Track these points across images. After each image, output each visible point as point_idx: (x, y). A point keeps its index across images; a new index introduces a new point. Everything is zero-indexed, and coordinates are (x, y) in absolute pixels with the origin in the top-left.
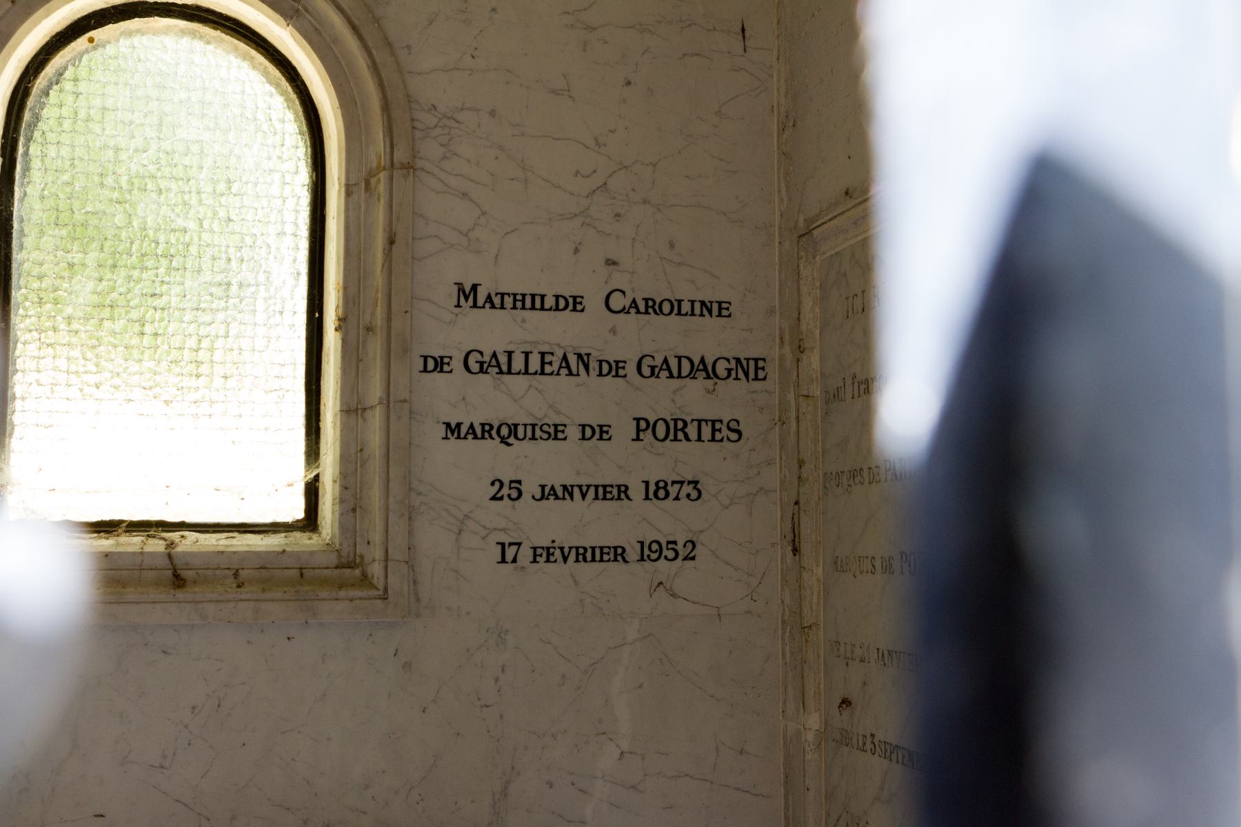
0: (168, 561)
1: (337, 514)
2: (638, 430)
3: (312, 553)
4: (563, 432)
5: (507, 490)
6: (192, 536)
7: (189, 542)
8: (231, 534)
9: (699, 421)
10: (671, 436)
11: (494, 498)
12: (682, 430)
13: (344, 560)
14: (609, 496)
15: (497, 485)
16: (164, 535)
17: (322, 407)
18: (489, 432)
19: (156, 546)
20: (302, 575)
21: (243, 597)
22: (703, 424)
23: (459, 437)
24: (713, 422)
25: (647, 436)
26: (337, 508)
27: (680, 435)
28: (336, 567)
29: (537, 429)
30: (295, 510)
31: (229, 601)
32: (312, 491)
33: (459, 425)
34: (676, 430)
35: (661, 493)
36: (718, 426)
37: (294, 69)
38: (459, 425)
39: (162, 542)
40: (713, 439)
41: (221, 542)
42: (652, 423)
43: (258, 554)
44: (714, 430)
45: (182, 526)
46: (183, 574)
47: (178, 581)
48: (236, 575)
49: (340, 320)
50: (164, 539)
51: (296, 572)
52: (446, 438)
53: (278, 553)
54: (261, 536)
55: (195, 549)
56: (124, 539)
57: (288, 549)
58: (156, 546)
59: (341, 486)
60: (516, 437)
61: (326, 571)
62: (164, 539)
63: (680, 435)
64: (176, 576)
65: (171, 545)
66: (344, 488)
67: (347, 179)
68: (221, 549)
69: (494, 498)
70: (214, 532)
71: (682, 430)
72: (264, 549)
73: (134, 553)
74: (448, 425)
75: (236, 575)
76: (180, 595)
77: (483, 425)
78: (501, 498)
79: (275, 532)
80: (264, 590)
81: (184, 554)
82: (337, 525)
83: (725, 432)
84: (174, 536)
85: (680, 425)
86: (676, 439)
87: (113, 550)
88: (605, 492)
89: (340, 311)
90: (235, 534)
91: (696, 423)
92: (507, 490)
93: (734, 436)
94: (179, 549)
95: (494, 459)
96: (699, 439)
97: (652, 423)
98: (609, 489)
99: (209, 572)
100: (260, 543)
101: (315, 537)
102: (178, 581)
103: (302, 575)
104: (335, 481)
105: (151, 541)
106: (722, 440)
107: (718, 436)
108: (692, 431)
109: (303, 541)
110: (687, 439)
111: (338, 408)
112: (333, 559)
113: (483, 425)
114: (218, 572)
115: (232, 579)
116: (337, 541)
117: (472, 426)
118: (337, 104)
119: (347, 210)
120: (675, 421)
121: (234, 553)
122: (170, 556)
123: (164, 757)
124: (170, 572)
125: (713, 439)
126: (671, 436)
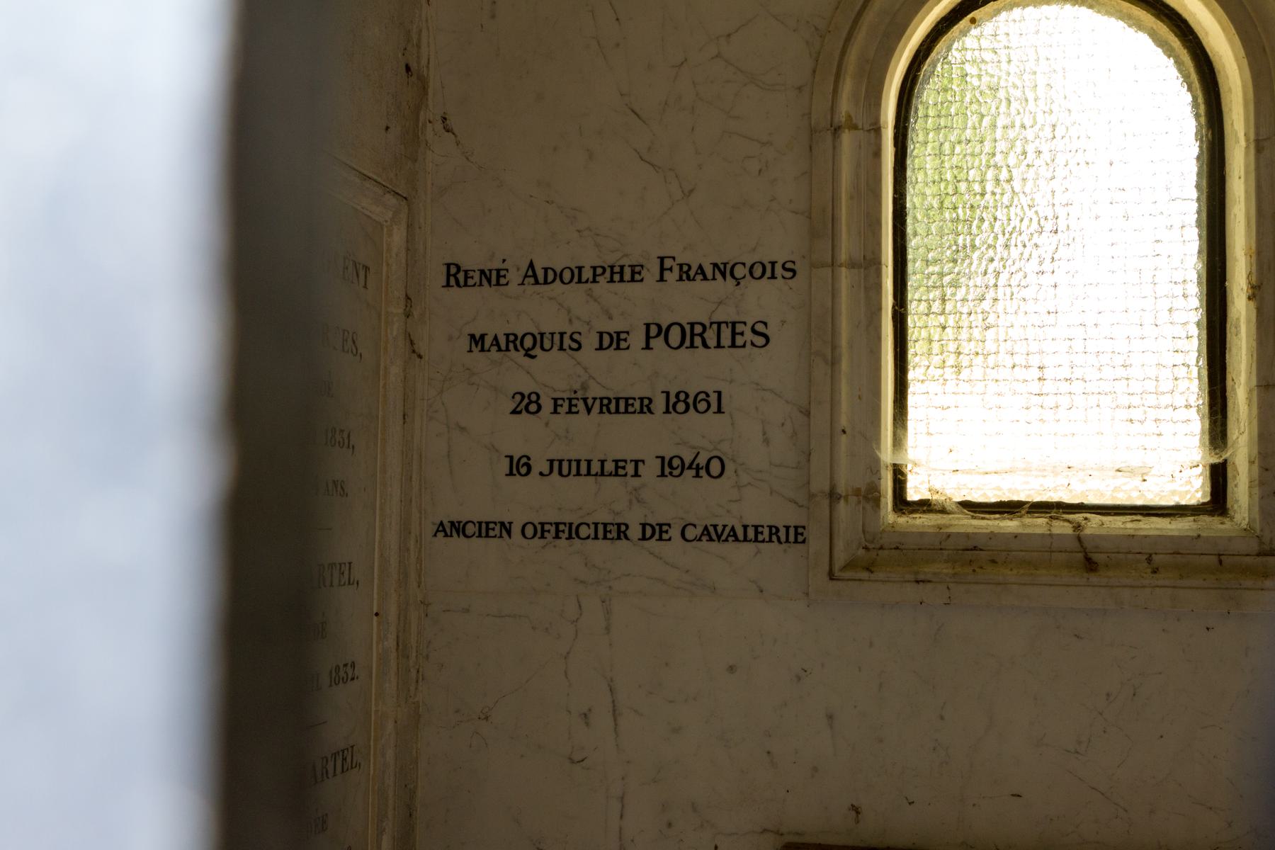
0: (1077, 544)
1: (1256, 498)
2: (648, 338)
3: (1230, 539)
4: (625, 340)
5: (527, 404)
6: (1095, 519)
7: (1095, 523)
8: (1135, 517)
9: (719, 324)
10: (687, 343)
11: (514, 412)
12: (701, 335)
13: (1267, 547)
14: (631, 409)
15: (518, 397)
16: (1071, 517)
17: (1229, 383)
18: (514, 342)
19: (1062, 528)
20: (1221, 562)
21: (1160, 583)
22: (723, 326)
23: (482, 350)
24: (734, 324)
25: (658, 343)
26: (1256, 490)
27: (698, 341)
28: (1258, 555)
29: (566, 338)
30: (1194, 490)
31: (1144, 587)
32: (1219, 476)
33: (482, 336)
34: (693, 335)
35: (681, 407)
36: (739, 328)
37: (1185, 22)
38: (482, 336)
39: (1066, 524)
40: (733, 345)
41: (1129, 525)
42: (664, 328)
43: (1171, 538)
44: (734, 334)
45: (1081, 508)
46: (1095, 557)
47: (1090, 565)
48: (1149, 560)
49: (1253, 287)
50: (1068, 521)
51: (1214, 559)
52: (470, 351)
53: (1192, 538)
54: (1168, 520)
55: (1103, 532)
56: (1028, 520)
57: (1203, 534)
58: (1062, 528)
59: (1261, 467)
60: (542, 348)
61: (1248, 559)
62: (1068, 521)
63: (698, 341)
64: (1088, 560)
65: (1078, 527)
66: (1265, 469)
67: (1257, 134)
68: (1132, 532)
69: (514, 412)
70: (1116, 514)
71: (701, 335)
72: (1176, 533)
73: (1043, 535)
74: (472, 336)
75: (1149, 560)
76: (1094, 579)
77: (507, 335)
78: (520, 412)
79: (1182, 515)
80: (1181, 577)
81: (1094, 537)
82: (1256, 509)
83: (749, 336)
84: (1078, 517)
85: (698, 329)
86: (692, 346)
87: (1021, 531)
88: (627, 405)
89: (1254, 279)
90: (1139, 517)
91: (715, 326)
92: (527, 404)
93: (760, 341)
94: (1088, 531)
95: (518, 374)
96: (719, 346)
97: (664, 328)
98: (631, 402)
99: (1121, 556)
100: (1169, 526)
101: (1226, 520)
102: (1090, 565)
103: (1221, 562)
104: (1251, 463)
105: (1056, 523)
106: (744, 346)
107: (739, 340)
108: (711, 336)
109: (1212, 525)
110: (705, 345)
111: (1254, 382)
112: (1254, 546)
113: (507, 335)
114: (1130, 556)
115: (1146, 564)
116: (1257, 526)
117: (496, 338)
118: (1242, 53)
119: (1257, 168)
120: (692, 325)
121: (1146, 537)
122: (1079, 539)
123: (1080, 743)
124: (1080, 556)
125: (733, 345)
126: (687, 343)
